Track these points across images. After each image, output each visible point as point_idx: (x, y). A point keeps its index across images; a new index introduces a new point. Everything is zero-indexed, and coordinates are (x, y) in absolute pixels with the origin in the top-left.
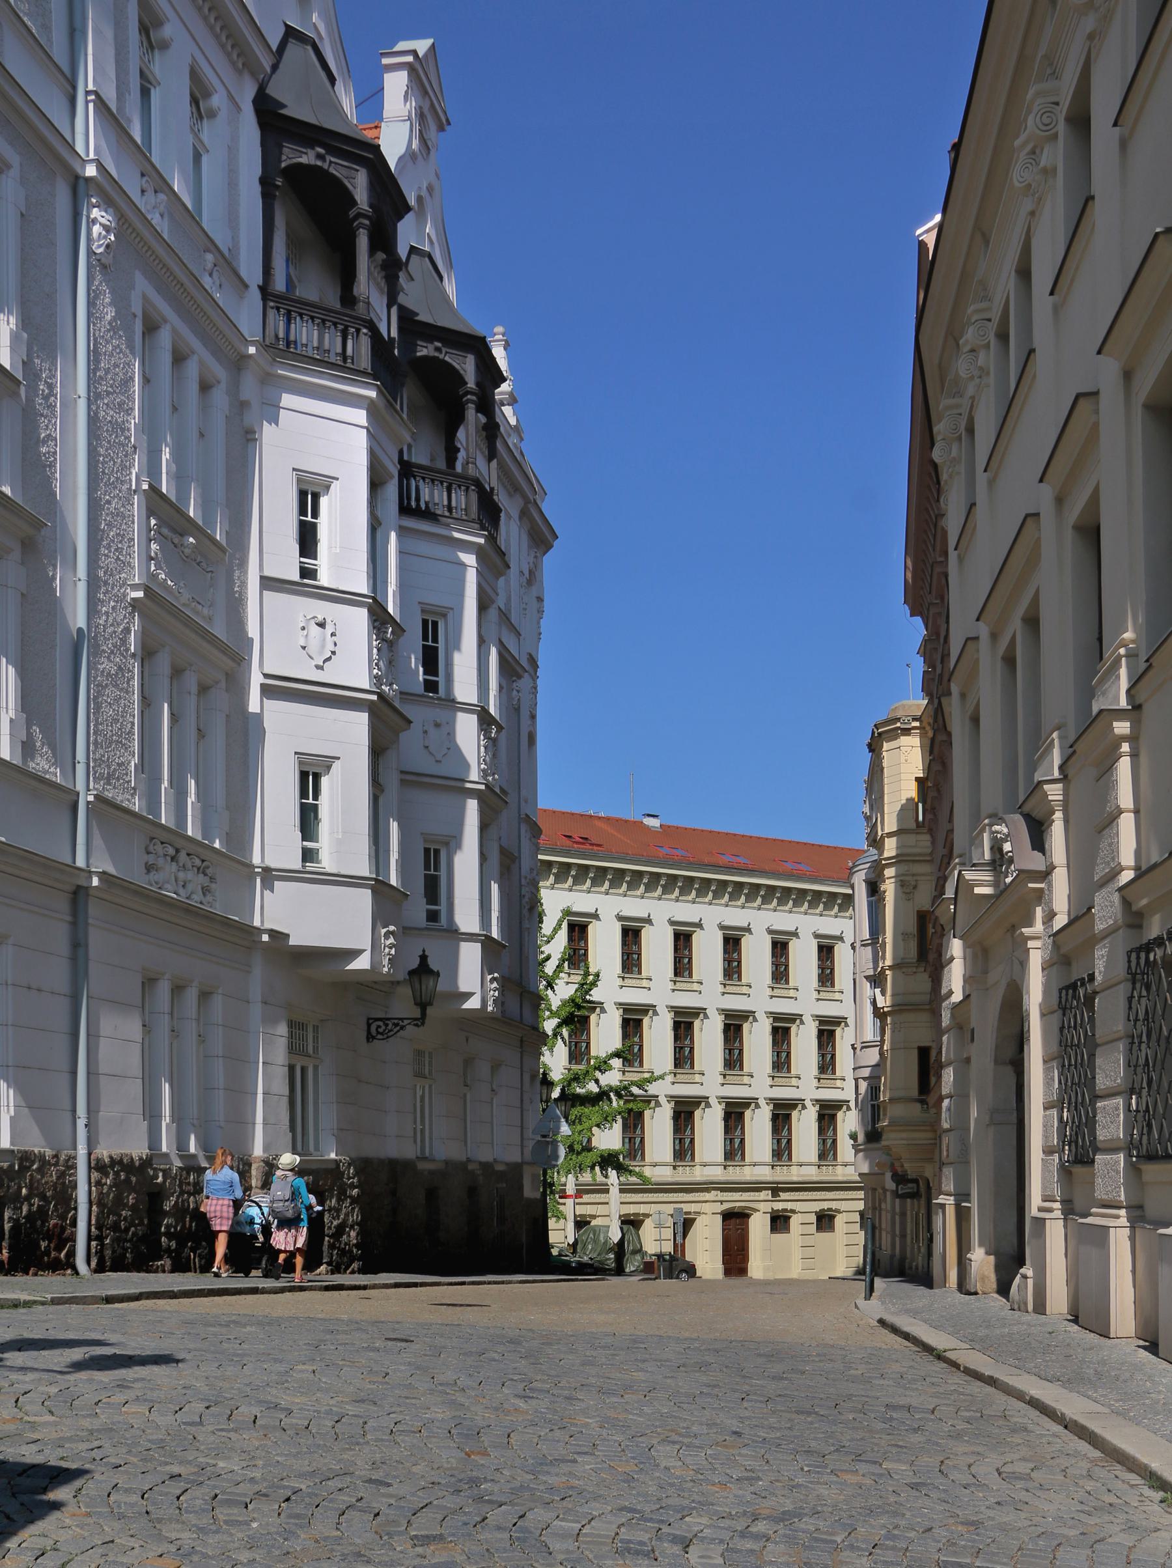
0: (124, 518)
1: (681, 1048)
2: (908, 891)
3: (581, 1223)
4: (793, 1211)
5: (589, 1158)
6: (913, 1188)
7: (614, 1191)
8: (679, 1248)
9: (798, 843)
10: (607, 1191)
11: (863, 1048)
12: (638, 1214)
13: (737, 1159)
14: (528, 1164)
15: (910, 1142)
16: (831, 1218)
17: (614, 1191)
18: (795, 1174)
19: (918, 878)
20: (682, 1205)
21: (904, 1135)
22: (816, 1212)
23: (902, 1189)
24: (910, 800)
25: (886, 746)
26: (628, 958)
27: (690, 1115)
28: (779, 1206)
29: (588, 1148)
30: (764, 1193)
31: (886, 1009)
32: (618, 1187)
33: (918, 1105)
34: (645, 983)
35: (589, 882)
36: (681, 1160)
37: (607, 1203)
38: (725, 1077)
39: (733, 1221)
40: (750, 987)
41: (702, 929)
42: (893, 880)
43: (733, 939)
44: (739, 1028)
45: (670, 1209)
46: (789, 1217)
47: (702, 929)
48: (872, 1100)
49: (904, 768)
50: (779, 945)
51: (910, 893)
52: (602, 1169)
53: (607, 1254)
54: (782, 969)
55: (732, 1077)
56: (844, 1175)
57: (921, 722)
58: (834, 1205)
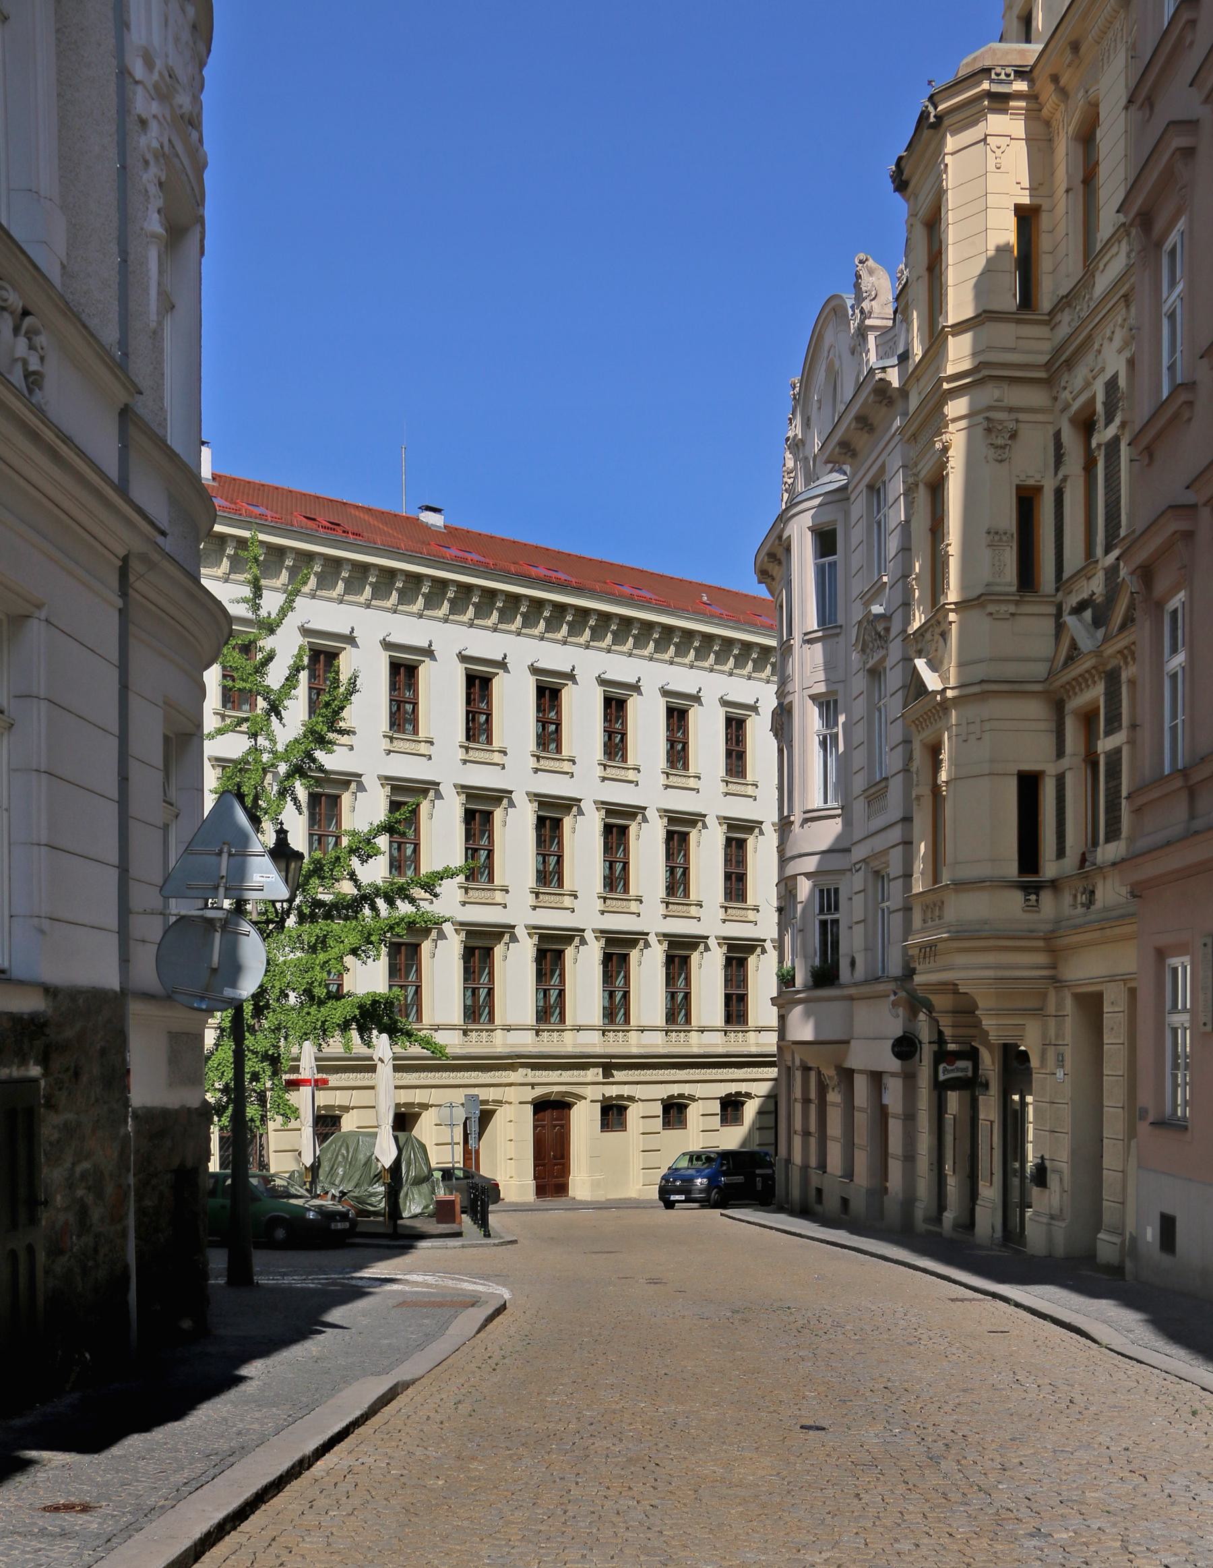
0: (326, 1021)
1: (475, 850)
2: (1000, 441)
3: (326, 1123)
4: (631, 1099)
5: (338, 1011)
6: (963, 1070)
7: (385, 1072)
8: (471, 1155)
9: (633, 569)
10: (372, 1069)
11: (806, 821)
12: (412, 1105)
13: (552, 1020)
14: (147, 996)
15: (1000, 973)
16: (682, 1108)
17: (385, 1072)
18: (634, 1044)
19: (1022, 417)
20: (475, 1091)
21: (990, 958)
22: (662, 1100)
23: (945, 1070)
24: (1002, 250)
25: (951, 143)
26: (399, 709)
27: (488, 952)
28: (613, 1091)
29: (338, 996)
30: (593, 1071)
31: (950, 694)
32: (391, 1063)
33: (1018, 896)
34: (423, 748)
35: (341, 585)
36: (474, 1021)
37: (372, 1088)
38: (537, 897)
39: (548, 1113)
40: (574, 762)
41: (507, 670)
42: (963, 424)
43: (550, 689)
44: (557, 824)
45: (458, 1096)
46: (626, 1108)
47: (507, 670)
48: (821, 911)
49: (994, 182)
50: (614, 703)
51: (1003, 447)
52: (362, 1030)
53: (371, 1184)
54: (618, 740)
55: (547, 897)
56: (700, 1046)
57: (1032, 82)
58: (686, 1089)
